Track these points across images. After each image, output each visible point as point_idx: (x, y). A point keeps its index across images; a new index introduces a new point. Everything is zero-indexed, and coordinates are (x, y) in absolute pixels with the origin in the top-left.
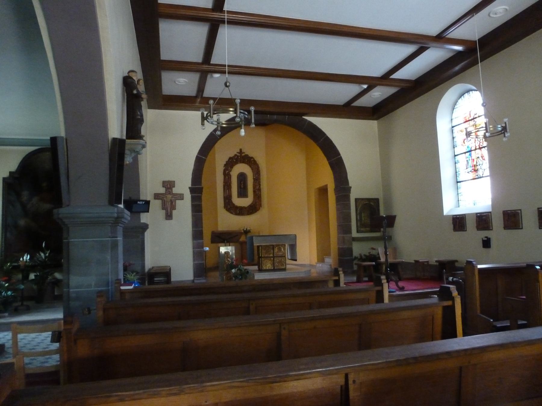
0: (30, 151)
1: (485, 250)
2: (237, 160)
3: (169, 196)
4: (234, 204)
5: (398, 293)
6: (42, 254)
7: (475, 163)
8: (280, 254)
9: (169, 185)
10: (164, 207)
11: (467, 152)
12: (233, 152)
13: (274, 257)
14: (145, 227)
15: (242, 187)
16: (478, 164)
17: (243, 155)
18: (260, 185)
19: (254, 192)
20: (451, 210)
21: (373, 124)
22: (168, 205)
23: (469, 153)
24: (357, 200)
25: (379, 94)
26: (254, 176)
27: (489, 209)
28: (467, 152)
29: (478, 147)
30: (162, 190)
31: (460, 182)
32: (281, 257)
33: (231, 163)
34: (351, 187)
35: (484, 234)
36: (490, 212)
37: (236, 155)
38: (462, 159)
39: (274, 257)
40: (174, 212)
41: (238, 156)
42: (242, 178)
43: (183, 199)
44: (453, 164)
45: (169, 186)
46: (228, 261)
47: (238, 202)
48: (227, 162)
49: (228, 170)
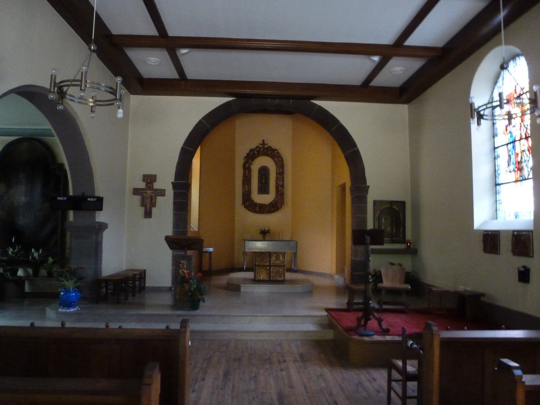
0: (11, 141)
1: (520, 284)
2: (258, 151)
3: (149, 192)
4: (253, 201)
5: (377, 338)
6: (11, 249)
7: (519, 159)
8: (278, 262)
9: (150, 179)
10: (143, 204)
11: (510, 143)
12: (254, 144)
13: (270, 266)
14: (103, 227)
15: (264, 182)
16: (523, 160)
17: (266, 146)
18: (283, 181)
19: (277, 188)
20: (485, 223)
21: (401, 111)
22: (148, 201)
23: (512, 145)
24: (375, 203)
25: (399, 70)
26: (277, 171)
27: (530, 227)
28: (510, 143)
29: (524, 137)
30: (142, 185)
31: (499, 185)
32: (279, 266)
33: (251, 156)
34: (369, 187)
35: (521, 261)
36: (531, 231)
37: (257, 147)
38: (502, 152)
39: (270, 266)
40: (154, 210)
41: (260, 148)
42: (264, 172)
43: (164, 195)
44: (489, 158)
45: (149, 180)
46: (183, 272)
47: (259, 198)
48: (247, 154)
49: (248, 163)
